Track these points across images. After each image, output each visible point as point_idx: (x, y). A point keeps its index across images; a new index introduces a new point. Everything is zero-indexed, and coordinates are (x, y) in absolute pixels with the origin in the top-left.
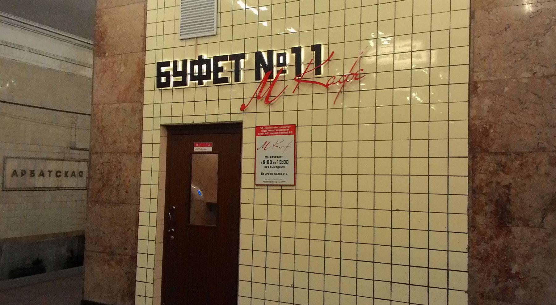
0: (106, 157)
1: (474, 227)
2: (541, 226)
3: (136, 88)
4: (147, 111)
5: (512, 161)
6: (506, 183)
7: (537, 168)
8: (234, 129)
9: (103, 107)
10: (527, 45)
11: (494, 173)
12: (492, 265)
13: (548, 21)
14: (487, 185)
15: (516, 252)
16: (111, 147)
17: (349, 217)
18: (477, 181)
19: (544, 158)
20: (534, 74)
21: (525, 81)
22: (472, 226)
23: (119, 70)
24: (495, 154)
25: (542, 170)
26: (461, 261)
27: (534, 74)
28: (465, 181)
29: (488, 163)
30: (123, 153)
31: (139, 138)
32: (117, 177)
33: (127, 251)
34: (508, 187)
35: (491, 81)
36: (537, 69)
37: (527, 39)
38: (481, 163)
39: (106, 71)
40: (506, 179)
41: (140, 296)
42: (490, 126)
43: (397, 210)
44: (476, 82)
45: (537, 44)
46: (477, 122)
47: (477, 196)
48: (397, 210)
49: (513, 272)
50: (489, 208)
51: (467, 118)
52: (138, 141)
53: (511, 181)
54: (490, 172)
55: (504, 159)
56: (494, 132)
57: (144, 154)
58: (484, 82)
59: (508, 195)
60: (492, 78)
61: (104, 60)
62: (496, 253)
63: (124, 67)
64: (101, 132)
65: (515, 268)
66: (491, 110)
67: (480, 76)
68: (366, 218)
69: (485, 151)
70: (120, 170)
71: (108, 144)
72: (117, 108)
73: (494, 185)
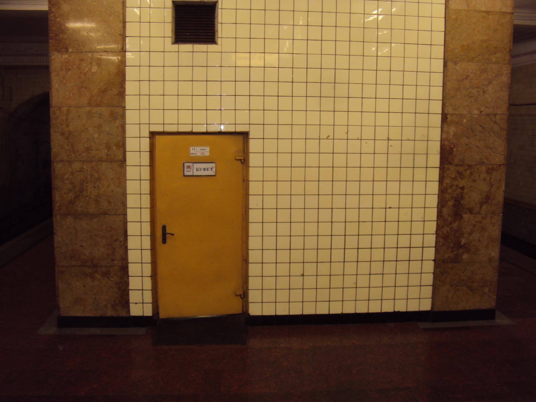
0: (76, 166)
1: (441, 216)
2: (479, 213)
3: (115, 91)
4: (130, 117)
5: (466, 171)
6: (461, 185)
7: (479, 175)
8: (245, 135)
9: (68, 111)
10: (478, 92)
11: (455, 179)
12: (450, 241)
13: (490, 77)
14: (451, 187)
15: (464, 230)
16: (84, 154)
17: (352, 215)
18: (445, 185)
19: (483, 168)
20: (481, 112)
21: (476, 116)
22: (440, 215)
23: (90, 70)
24: (456, 165)
25: (483, 176)
26: (431, 240)
27: (481, 112)
28: (436, 184)
29: (452, 171)
30: (101, 160)
31: (122, 145)
32: (94, 187)
33: (115, 262)
34: (463, 188)
35: (455, 114)
36: (483, 109)
37: (478, 87)
38: (448, 172)
39: (70, 70)
40: (462, 183)
41: (136, 303)
42: (454, 146)
43: (390, 208)
44: (446, 114)
45: (484, 92)
46: (446, 143)
47: (444, 195)
48: (390, 208)
49: (462, 243)
50: (451, 203)
51: (439, 139)
52: (122, 149)
53: (465, 184)
54: (453, 178)
55: (461, 169)
56: (457, 150)
57: (128, 162)
58: (452, 114)
59: (462, 193)
60: (457, 113)
61: (66, 56)
62: (453, 232)
63: (96, 67)
64: (67, 138)
65: (463, 241)
66: (455, 135)
67: (449, 110)
68: (366, 215)
69: (450, 163)
70: (99, 179)
71: (78, 151)
72: (90, 112)
73: (454, 187)
